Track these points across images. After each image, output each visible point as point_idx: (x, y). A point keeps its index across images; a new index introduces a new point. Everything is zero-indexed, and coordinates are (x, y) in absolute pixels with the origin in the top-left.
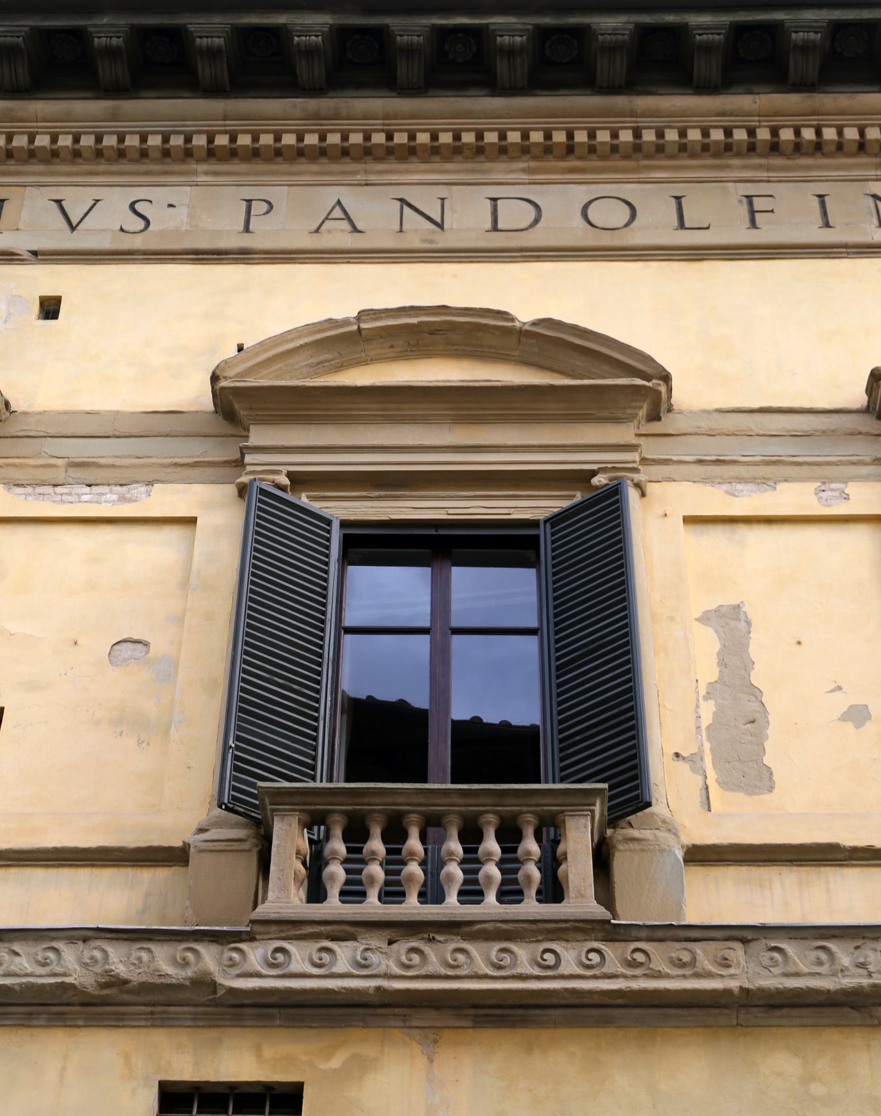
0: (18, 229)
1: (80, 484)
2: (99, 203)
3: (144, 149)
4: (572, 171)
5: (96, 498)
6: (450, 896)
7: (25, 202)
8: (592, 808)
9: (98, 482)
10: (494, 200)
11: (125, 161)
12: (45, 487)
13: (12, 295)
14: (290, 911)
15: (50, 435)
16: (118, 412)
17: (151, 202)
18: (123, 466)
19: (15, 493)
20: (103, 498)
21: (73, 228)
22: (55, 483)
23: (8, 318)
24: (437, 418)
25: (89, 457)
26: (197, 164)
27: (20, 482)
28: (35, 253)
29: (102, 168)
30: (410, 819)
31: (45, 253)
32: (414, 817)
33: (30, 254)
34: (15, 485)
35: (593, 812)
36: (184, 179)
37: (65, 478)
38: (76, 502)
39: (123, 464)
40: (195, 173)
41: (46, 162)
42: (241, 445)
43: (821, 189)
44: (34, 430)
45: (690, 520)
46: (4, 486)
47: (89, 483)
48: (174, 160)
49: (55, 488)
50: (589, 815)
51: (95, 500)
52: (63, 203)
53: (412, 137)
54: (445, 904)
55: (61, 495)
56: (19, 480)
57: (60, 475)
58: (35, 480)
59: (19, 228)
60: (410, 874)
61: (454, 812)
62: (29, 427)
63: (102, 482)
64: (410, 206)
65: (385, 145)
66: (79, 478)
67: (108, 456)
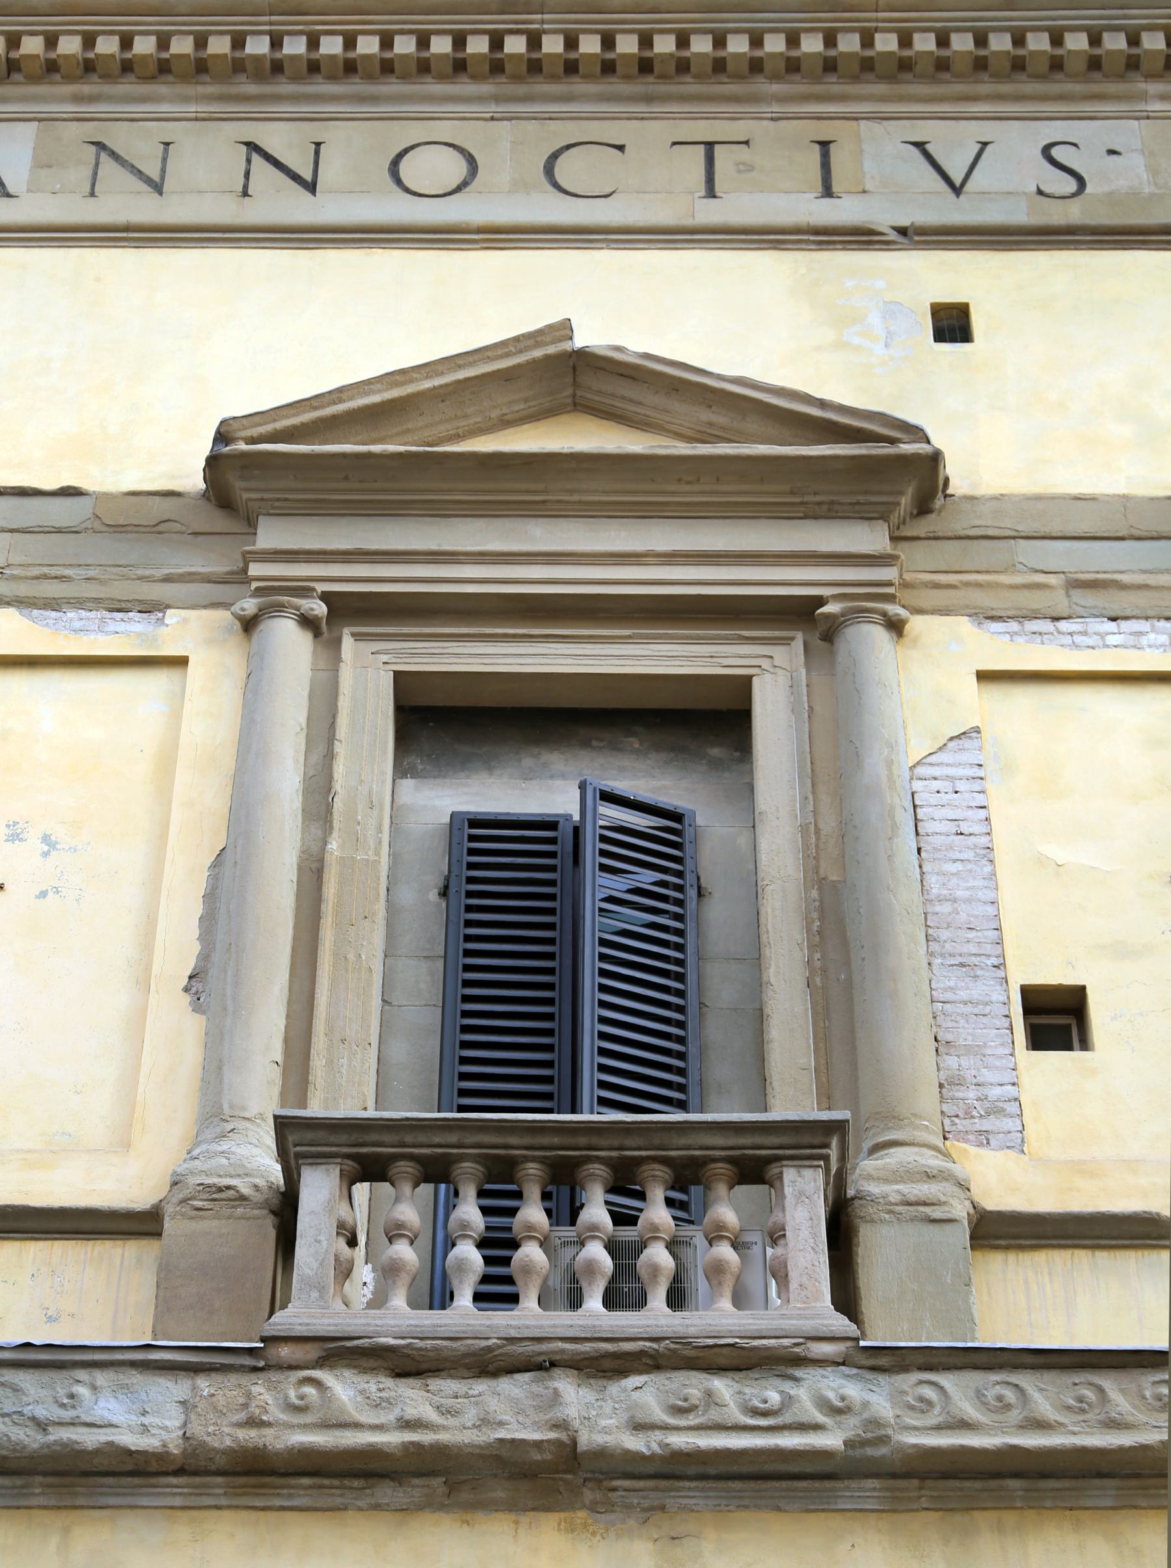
0: (864, 192)
1: (1098, 617)
2: (989, 148)
3: (201, 59)
4: (362, 99)
5: (1131, 640)
6: (527, 1297)
7: (865, 147)
8: (824, 1151)
9: (1128, 613)
10: (710, 146)
11: (1024, 77)
12: (1038, 621)
13: (884, 302)
14: (326, 1321)
15: (1023, 534)
16: (1125, 497)
17: (1075, 145)
18: (1163, 587)
19: (992, 630)
20: (1144, 641)
21: (957, 190)
22: (1054, 615)
23: (888, 340)
24: (589, 508)
25: (1098, 572)
26: (1146, 82)
27: (995, 613)
28: (902, 231)
29: (985, 88)
30: (525, 1172)
31: (923, 231)
32: (533, 1169)
33: (895, 233)
34: (987, 618)
35: (826, 1158)
36: (1123, 107)
37: (1070, 607)
38: (1099, 647)
39: (1161, 583)
40: (1143, 97)
41: (890, 78)
42: (241, 550)
43: (825, 131)
44: (993, 527)
45: (984, 677)
46: (971, 619)
47: (1113, 614)
48: (1106, 76)
49: (1057, 624)
50: (819, 1166)
51: (1132, 643)
52: (928, 147)
53: (905, 41)
54: (519, 1310)
55: (1071, 634)
56: (992, 609)
57: (1059, 601)
58: (1020, 609)
59: (866, 189)
60: (590, 1261)
61: (598, 1159)
62: (985, 521)
63: (1134, 613)
64: (114, 155)
65: (898, 55)
66: (1095, 607)
67: (1131, 571)
